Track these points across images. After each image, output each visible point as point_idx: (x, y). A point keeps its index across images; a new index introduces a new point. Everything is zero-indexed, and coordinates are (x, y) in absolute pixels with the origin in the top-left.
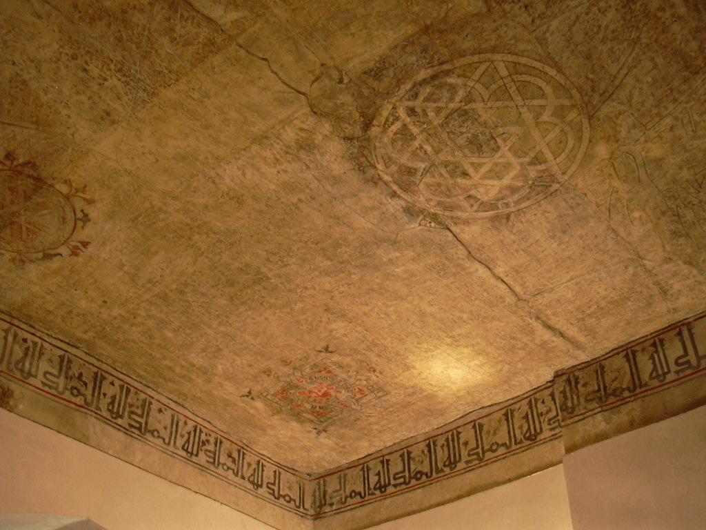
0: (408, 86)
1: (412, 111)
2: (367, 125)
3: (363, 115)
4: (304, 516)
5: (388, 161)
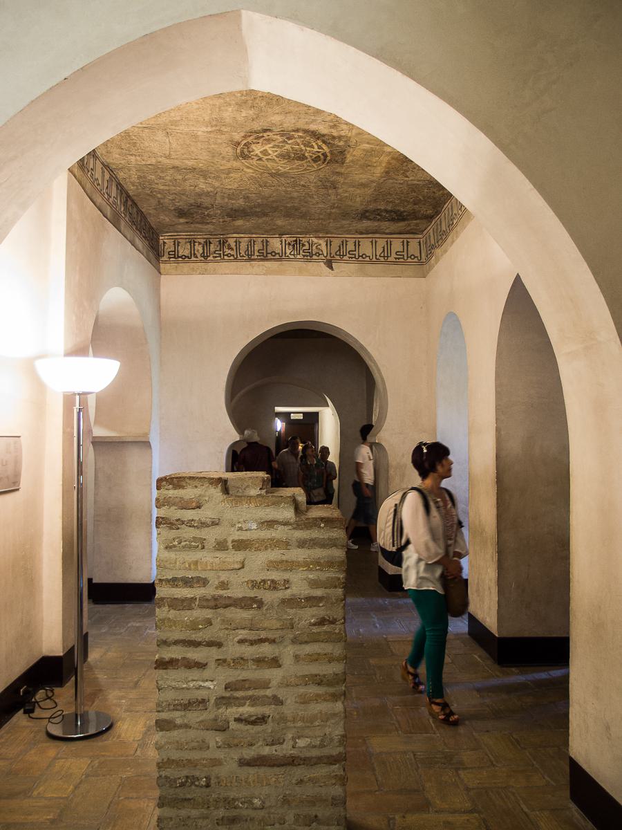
0: (329, 154)
1: (319, 152)
2: (324, 142)
3: (329, 143)
4: (94, 517)
5: (301, 137)
